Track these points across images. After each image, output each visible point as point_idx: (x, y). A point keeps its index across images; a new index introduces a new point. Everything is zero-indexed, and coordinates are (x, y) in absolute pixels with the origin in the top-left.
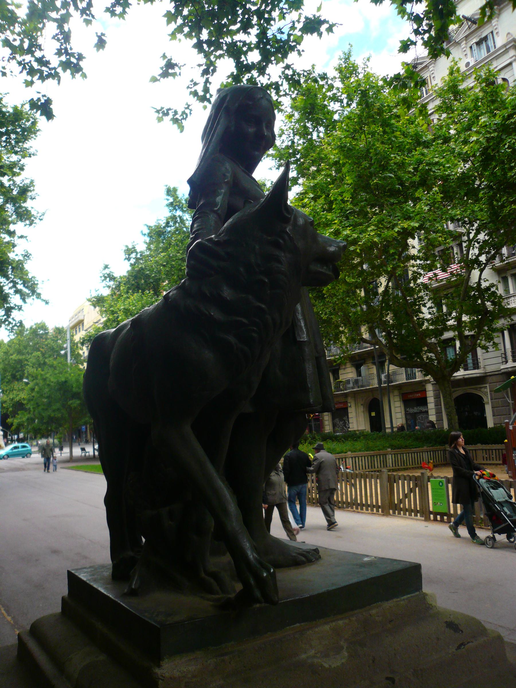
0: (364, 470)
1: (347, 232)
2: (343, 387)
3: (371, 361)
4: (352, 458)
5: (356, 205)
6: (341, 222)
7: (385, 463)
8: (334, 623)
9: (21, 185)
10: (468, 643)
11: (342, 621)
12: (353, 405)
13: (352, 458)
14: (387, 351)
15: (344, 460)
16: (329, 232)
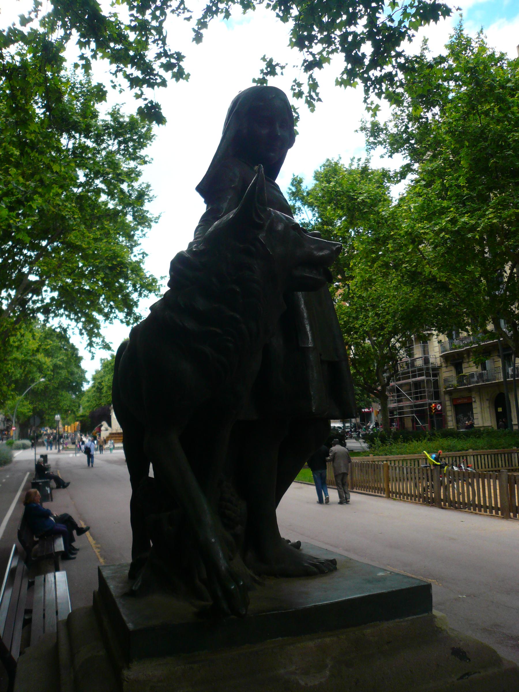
0: (484, 469)
1: (465, 219)
2: (467, 381)
3: (497, 354)
4: (474, 456)
5: (473, 190)
6: (457, 209)
7: (510, 463)
8: (320, 640)
9: (139, 189)
10: (475, 673)
11: (329, 639)
12: (477, 400)
13: (474, 456)
14: (513, 343)
15: (465, 458)
16: (446, 221)
